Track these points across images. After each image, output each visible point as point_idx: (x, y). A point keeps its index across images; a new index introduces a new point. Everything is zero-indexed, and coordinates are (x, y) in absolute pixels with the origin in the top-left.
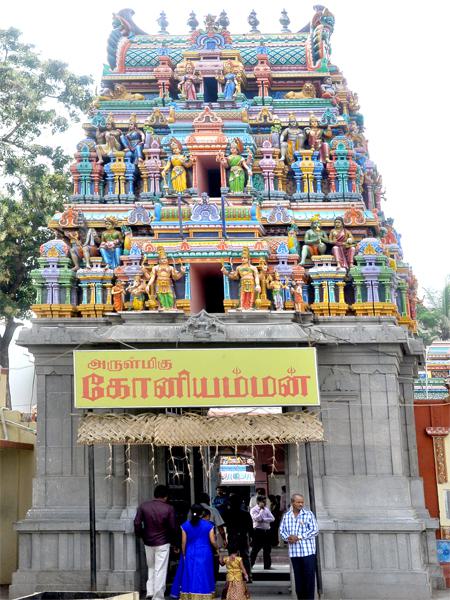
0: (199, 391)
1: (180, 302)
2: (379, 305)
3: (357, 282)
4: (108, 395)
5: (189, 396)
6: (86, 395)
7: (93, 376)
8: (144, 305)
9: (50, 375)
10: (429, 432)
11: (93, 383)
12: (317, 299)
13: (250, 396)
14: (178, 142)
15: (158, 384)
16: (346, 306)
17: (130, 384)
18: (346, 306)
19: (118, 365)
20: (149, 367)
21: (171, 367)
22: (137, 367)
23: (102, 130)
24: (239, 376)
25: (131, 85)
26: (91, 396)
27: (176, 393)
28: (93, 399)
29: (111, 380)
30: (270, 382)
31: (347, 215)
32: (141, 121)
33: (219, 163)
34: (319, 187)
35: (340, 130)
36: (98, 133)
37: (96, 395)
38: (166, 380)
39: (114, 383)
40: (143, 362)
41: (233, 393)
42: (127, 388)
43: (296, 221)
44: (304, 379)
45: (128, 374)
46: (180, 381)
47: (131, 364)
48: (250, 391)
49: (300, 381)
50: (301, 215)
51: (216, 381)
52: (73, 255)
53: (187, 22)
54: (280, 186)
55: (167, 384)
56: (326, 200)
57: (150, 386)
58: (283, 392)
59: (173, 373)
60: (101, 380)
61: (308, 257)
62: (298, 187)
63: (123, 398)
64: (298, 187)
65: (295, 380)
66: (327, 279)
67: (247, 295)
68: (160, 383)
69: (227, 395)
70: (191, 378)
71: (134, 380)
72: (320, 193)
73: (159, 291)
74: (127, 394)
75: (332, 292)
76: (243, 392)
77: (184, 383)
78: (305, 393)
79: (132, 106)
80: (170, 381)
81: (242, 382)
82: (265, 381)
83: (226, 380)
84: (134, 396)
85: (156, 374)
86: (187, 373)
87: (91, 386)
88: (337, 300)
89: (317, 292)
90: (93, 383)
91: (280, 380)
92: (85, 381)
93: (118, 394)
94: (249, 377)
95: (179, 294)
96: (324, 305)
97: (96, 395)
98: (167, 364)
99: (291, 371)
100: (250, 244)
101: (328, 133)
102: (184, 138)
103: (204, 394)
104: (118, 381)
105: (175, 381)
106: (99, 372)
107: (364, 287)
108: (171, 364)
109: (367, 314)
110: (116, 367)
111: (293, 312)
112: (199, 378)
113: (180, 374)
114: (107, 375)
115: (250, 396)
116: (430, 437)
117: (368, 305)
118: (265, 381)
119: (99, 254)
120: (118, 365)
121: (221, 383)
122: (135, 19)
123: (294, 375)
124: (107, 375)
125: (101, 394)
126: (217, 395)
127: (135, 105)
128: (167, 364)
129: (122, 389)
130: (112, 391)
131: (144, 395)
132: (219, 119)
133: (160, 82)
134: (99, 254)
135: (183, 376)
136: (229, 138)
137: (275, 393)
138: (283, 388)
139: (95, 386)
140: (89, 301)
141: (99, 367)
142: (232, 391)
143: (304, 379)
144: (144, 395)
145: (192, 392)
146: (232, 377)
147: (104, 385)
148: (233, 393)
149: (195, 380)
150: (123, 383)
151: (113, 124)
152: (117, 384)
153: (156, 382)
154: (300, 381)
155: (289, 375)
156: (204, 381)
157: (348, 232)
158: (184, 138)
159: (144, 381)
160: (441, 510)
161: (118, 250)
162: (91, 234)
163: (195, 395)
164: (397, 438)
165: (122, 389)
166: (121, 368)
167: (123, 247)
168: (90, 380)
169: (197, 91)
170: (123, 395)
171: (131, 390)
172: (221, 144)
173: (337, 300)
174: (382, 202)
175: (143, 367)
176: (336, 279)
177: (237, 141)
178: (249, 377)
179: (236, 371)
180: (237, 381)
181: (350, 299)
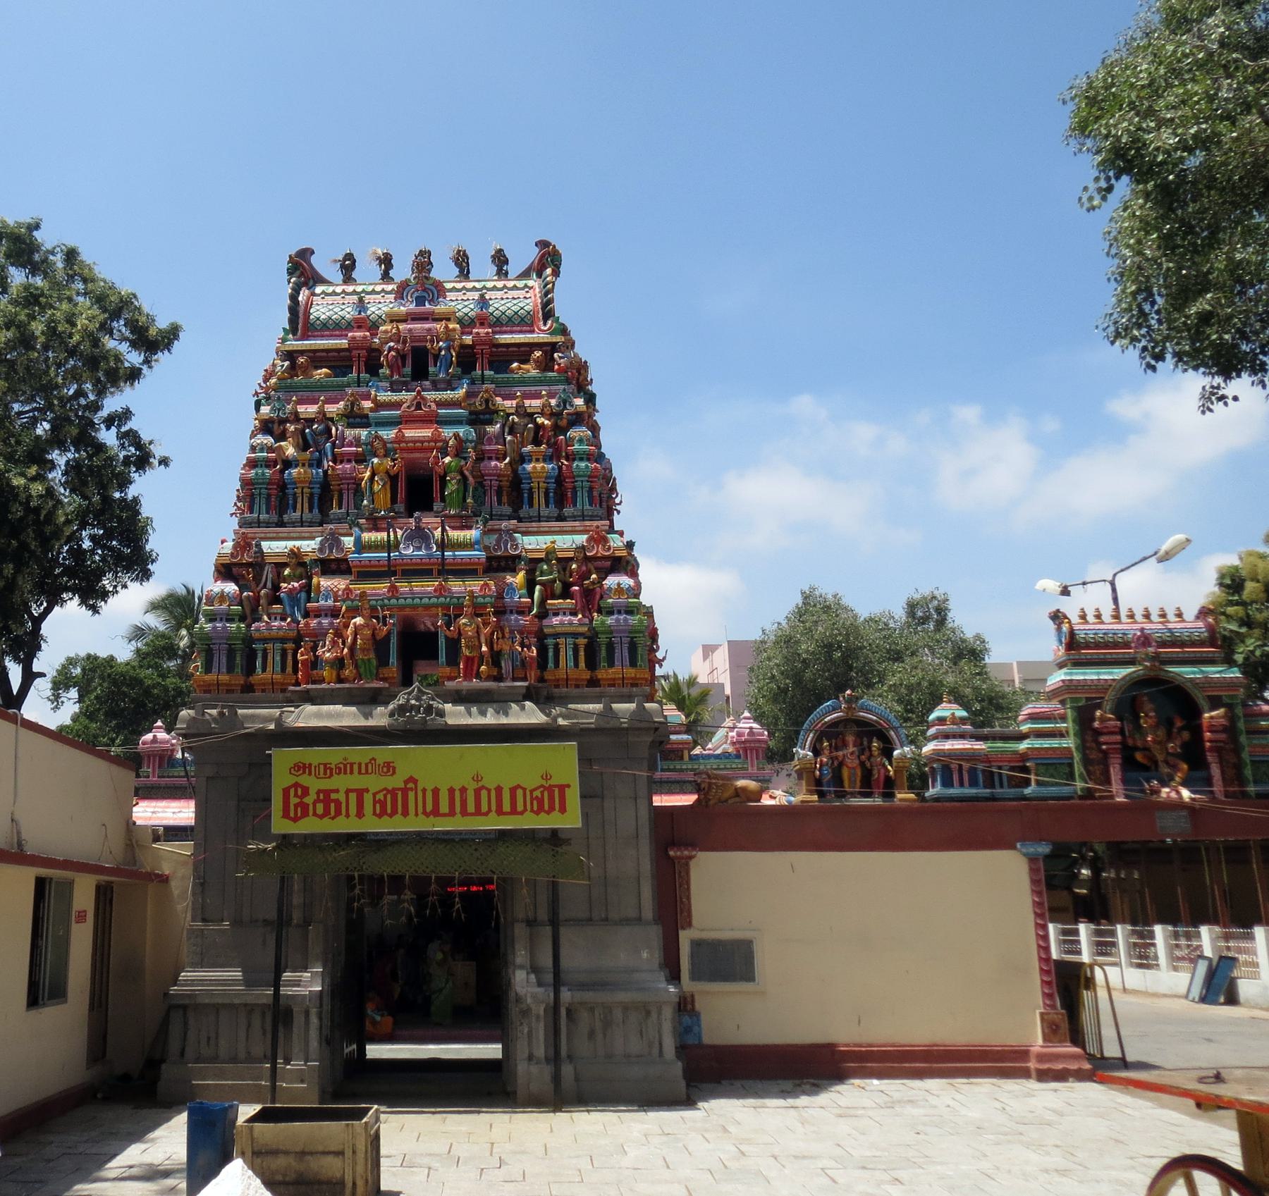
0: (429, 807)
1: (385, 672)
2: (630, 672)
3: (603, 639)
4: (315, 814)
5: (417, 814)
6: (286, 815)
7: (296, 785)
8: (338, 675)
9: (212, 778)
10: (671, 853)
11: (296, 795)
12: (551, 665)
13: (493, 814)
14: (381, 439)
15: (378, 797)
16: (587, 675)
17: (341, 796)
18: (587, 675)
19: (329, 771)
20: (367, 772)
21: (394, 773)
22: (352, 772)
23: (283, 422)
24: (480, 784)
25: (317, 358)
26: (292, 814)
27: (400, 810)
28: (295, 820)
29: (319, 792)
30: (520, 793)
31: (588, 540)
32: (332, 409)
33: (432, 469)
34: (552, 501)
35: (579, 419)
36: (276, 426)
37: (299, 815)
38: (388, 791)
39: (322, 796)
40: (360, 764)
41: (509, 810)
42: (338, 803)
43: (527, 551)
44: (563, 788)
45: (340, 782)
46: (405, 791)
47: (345, 768)
48: (494, 807)
49: (557, 791)
50: (533, 543)
51: (451, 791)
52: (245, 603)
53: (827, 589)
54: (505, 499)
55: (389, 797)
56: (561, 518)
57: (368, 799)
58: (535, 808)
59: (396, 782)
60: (306, 791)
61: (543, 602)
62: (526, 500)
63: (333, 818)
64: (526, 500)
65: (550, 789)
66: (566, 635)
67: (469, 660)
68: (380, 796)
69: (464, 813)
70: (420, 787)
71: (348, 791)
72: (552, 509)
73: (360, 656)
74: (338, 813)
75: (570, 653)
76: (484, 808)
77: (411, 795)
78: (563, 809)
79: (321, 387)
80: (393, 792)
81: (484, 794)
82: (513, 791)
83: (463, 790)
84: (348, 816)
85: (375, 783)
86: (415, 781)
87: (294, 800)
88: (576, 665)
89: (551, 654)
90: (296, 795)
91: (531, 792)
92: (286, 792)
93: (326, 813)
94: (492, 786)
95: (383, 660)
96: (561, 674)
97: (299, 815)
98: (389, 768)
99: (546, 777)
100: (475, 585)
101: (563, 423)
102: (389, 434)
103: (436, 812)
104: (327, 793)
105: (400, 794)
106: (305, 780)
107: (611, 647)
108: (394, 768)
109: (614, 685)
110: (325, 773)
111: (525, 684)
112: (430, 787)
113: (406, 782)
114: (314, 784)
115: (493, 814)
116: (672, 860)
117: (613, 673)
118: (513, 791)
119: (278, 600)
120: (329, 771)
121: (457, 794)
122: (315, 261)
123: (550, 782)
124: (314, 784)
125: (305, 814)
126: (452, 813)
127: (322, 386)
128: (389, 768)
129: (333, 805)
130: (320, 808)
131: (360, 814)
132: (434, 406)
133: (355, 353)
134: (278, 600)
135: (411, 785)
136: (447, 432)
137: (525, 810)
138: (535, 803)
139: (297, 800)
140: (264, 670)
141: (304, 772)
142: (471, 808)
143: (563, 788)
144: (360, 814)
145: (420, 809)
146: (472, 786)
147: (309, 800)
148: (509, 810)
149: (424, 791)
150: (333, 796)
151: (296, 414)
152: (326, 797)
153: (374, 795)
154: (557, 791)
155: (544, 783)
156: (436, 792)
157: (589, 565)
158: (389, 434)
159: (360, 793)
160: (682, 968)
161: (303, 595)
162: (268, 573)
163: (425, 813)
164: (647, 866)
165: (333, 805)
166: (331, 775)
167: (309, 592)
168: (292, 792)
169: (404, 366)
170: (333, 813)
171: (344, 806)
172: (436, 442)
173: (576, 665)
174: (616, 517)
175: (360, 773)
176: (575, 635)
177: (456, 436)
178: (492, 786)
179: (477, 778)
180: (477, 792)
181: (592, 664)
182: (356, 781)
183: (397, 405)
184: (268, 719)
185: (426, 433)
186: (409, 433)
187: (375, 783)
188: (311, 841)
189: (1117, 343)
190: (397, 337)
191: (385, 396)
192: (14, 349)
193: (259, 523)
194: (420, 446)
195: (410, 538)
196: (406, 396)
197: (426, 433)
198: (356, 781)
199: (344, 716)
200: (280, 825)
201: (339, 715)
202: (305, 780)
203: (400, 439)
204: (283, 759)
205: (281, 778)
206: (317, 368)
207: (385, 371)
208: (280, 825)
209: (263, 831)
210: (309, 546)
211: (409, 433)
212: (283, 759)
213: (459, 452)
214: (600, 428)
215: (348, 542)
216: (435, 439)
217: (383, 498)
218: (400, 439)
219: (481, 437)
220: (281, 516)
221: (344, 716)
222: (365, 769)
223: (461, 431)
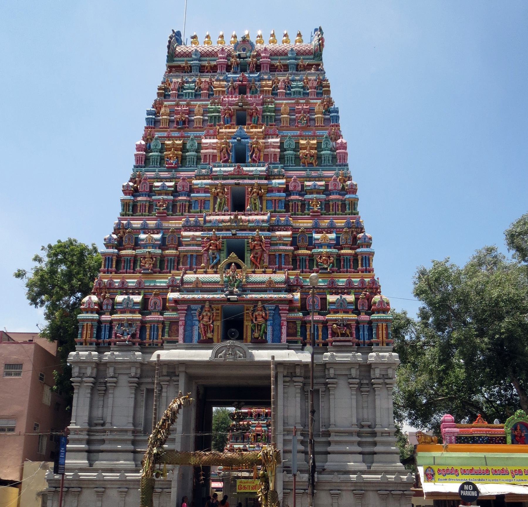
45: (246, 485)
47: (247, 482)
57: (250, 487)
59: (254, 485)
85: (251, 485)
106: (241, 484)
124: (243, 485)
128: (254, 483)
136: (263, 429)
152: (244, 487)
159: (249, 486)
182: (249, 484)
183: (255, 424)
184: (235, 474)
185: (260, 429)
186: (257, 429)
187: (251, 485)
188: (241, 493)
189: (38, 306)
190: (255, 412)
191: (253, 422)
192: (275, 229)
193: (233, 442)
194: (258, 431)
195: (257, 446)
196: (257, 422)
197: (260, 429)
198: (249, 484)
199: (246, 474)
200: (238, 491)
201: (246, 474)
202: (241, 484)
203: (256, 430)
204: (238, 481)
205: (238, 484)
206: (172, 291)
207: (253, 417)
208: (238, 491)
209: (235, 491)
210: (241, 446)
211: (257, 429)
212: (238, 481)
213: (265, 432)
214: (71, 242)
215: (247, 446)
216: (261, 430)
217: (253, 440)
218: (256, 430)
219: (268, 429)
220: (180, 254)
221: (246, 474)
222: (250, 483)
223: (265, 428)
